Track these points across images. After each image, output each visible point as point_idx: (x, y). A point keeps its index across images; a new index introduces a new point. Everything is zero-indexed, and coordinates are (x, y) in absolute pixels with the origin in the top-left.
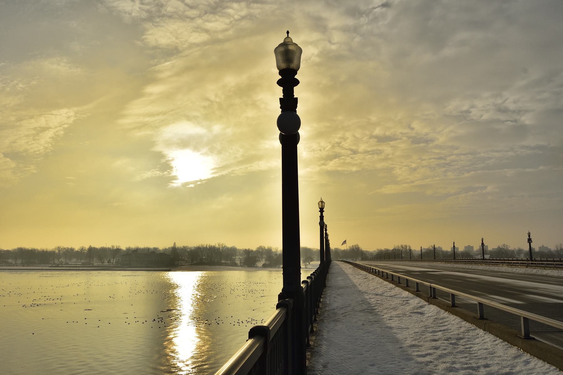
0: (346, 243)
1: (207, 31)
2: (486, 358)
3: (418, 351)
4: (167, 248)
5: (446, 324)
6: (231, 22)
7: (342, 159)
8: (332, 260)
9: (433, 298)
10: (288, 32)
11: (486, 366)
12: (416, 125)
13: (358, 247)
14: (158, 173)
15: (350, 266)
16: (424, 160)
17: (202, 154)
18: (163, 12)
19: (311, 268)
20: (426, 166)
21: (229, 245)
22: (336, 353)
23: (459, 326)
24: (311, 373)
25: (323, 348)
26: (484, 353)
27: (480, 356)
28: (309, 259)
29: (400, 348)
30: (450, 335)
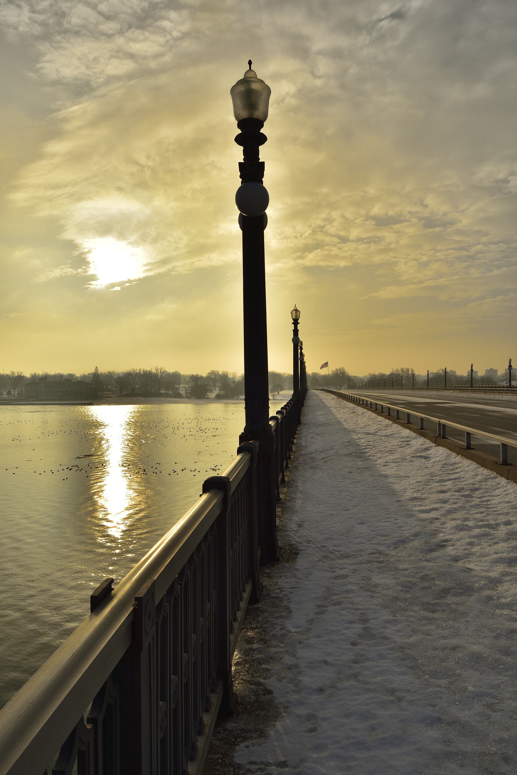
0: (327, 366)
1: (132, 56)
2: (507, 514)
3: (421, 506)
4: (86, 374)
5: (457, 471)
6: (167, 42)
7: (326, 250)
8: (308, 388)
9: (441, 438)
10: (250, 63)
11: (508, 523)
12: (431, 201)
13: (344, 371)
14: (69, 271)
15: (333, 396)
16: (440, 251)
17: (130, 243)
18: (66, 25)
19: (281, 400)
20: (441, 260)
21: (170, 370)
22: (314, 508)
23: (475, 473)
24: (282, 534)
25: (297, 503)
26: (505, 507)
27: (499, 511)
28: (280, 388)
29: (398, 501)
30: (462, 484)
